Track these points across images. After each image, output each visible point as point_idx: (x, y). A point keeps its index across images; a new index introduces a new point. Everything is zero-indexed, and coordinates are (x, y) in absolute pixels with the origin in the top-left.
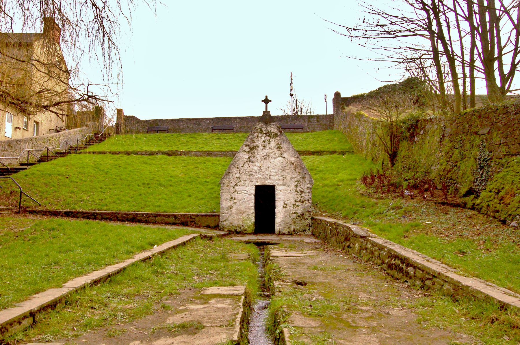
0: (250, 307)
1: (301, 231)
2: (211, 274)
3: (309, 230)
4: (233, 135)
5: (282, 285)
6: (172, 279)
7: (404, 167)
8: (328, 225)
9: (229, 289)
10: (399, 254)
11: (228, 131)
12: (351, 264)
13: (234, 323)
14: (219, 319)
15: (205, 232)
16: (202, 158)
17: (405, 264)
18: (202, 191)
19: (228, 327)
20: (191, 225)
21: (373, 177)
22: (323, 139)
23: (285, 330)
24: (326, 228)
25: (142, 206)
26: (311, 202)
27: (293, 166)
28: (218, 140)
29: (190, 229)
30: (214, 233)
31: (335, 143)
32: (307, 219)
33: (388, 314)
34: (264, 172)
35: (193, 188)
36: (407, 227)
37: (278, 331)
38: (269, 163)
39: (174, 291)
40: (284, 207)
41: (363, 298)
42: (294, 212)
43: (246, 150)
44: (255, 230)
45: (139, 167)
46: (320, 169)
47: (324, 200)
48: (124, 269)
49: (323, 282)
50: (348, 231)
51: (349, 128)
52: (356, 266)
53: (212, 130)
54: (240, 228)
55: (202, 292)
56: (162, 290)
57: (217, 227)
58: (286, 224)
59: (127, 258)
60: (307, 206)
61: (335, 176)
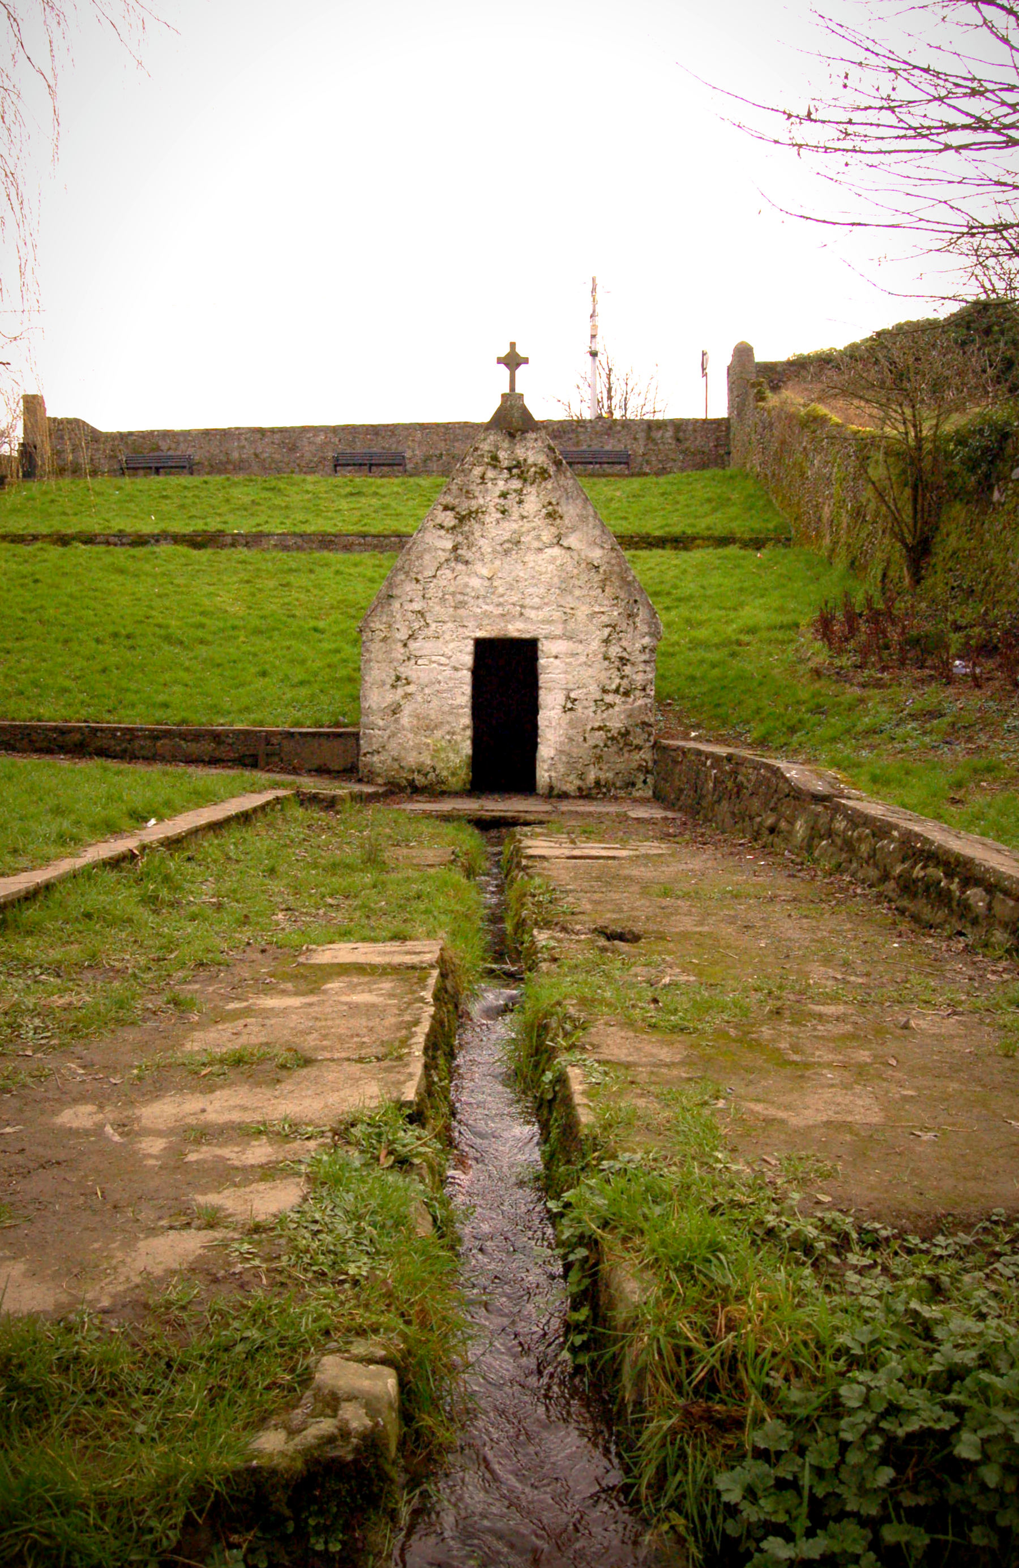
0: (456, 1007)
1: (618, 784)
2: (332, 906)
3: (645, 782)
4: (404, 483)
5: (559, 941)
6: (205, 919)
7: (953, 588)
8: (709, 763)
9: (388, 949)
10: (940, 846)
11: (386, 468)
12: (782, 881)
13: (406, 1051)
14: (356, 1039)
15: (310, 784)
16: (302, 556)
17: (957, 880)
18: (303, 662)
19: (384, 1064)
20: (268, 764)
21: (852, 618)
22: (693, 497)
23: (574, 1073)
24: (702, 775)
25: (110, 704)
26: (652, 693)
27: (597, 578)
28: (354, 499)
29: (261, 777)
30: (341, 789)
31: (733, 511)
32: (639, 748)
33: (906, 1026)
34: (502, 596)
35: (274, 650)
36: (960, 773)
37: (549, 1076)
38: (520, 566)
39: (210, 956)
40: (566, 710)
41: (823, 981)
42: (597, 725)
43: (445, 524)
44: (473, 783)
45: (99, 585)
46: (678, 593)
47: (695, 691)
48: (48, 887)
49: (696, 933)
50: (774, 780)
51: (778, 459)
52: (800, 888)
53: (336, 466)
54: (426, 775)
55: (302, 959)
56: (171, 952)
57: (351, 771)
58: (571, 765)
59: (60, 857)
60: (640, 707)
61: (732, 615)
